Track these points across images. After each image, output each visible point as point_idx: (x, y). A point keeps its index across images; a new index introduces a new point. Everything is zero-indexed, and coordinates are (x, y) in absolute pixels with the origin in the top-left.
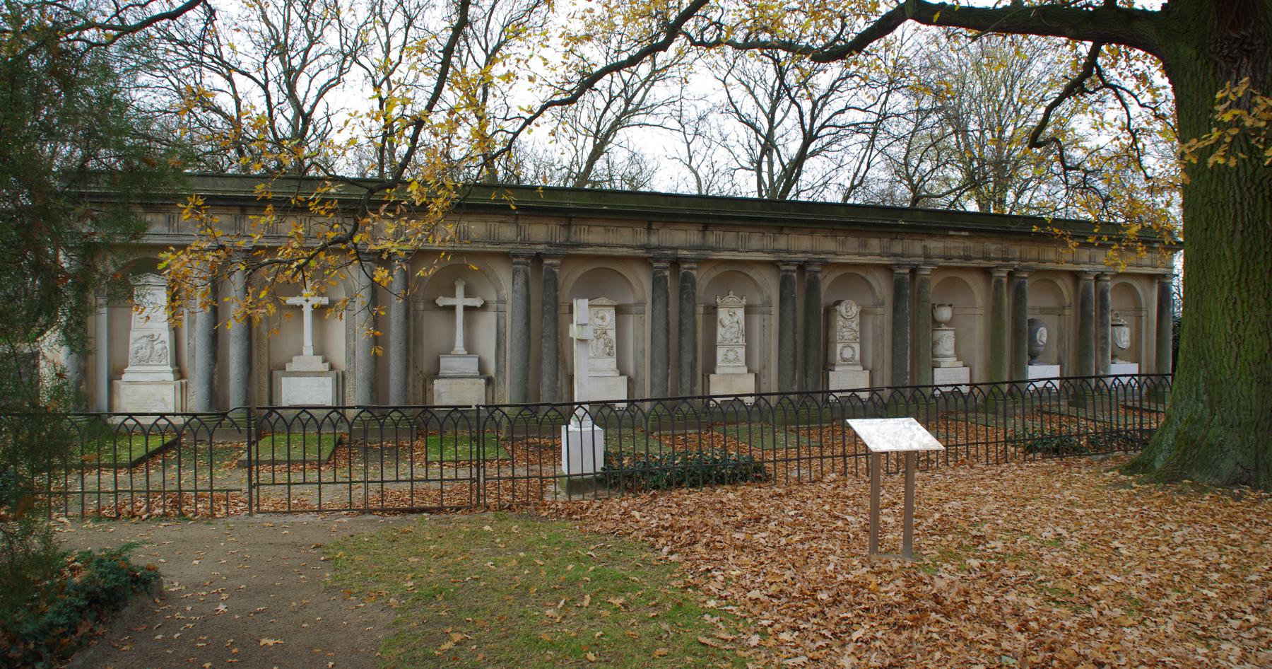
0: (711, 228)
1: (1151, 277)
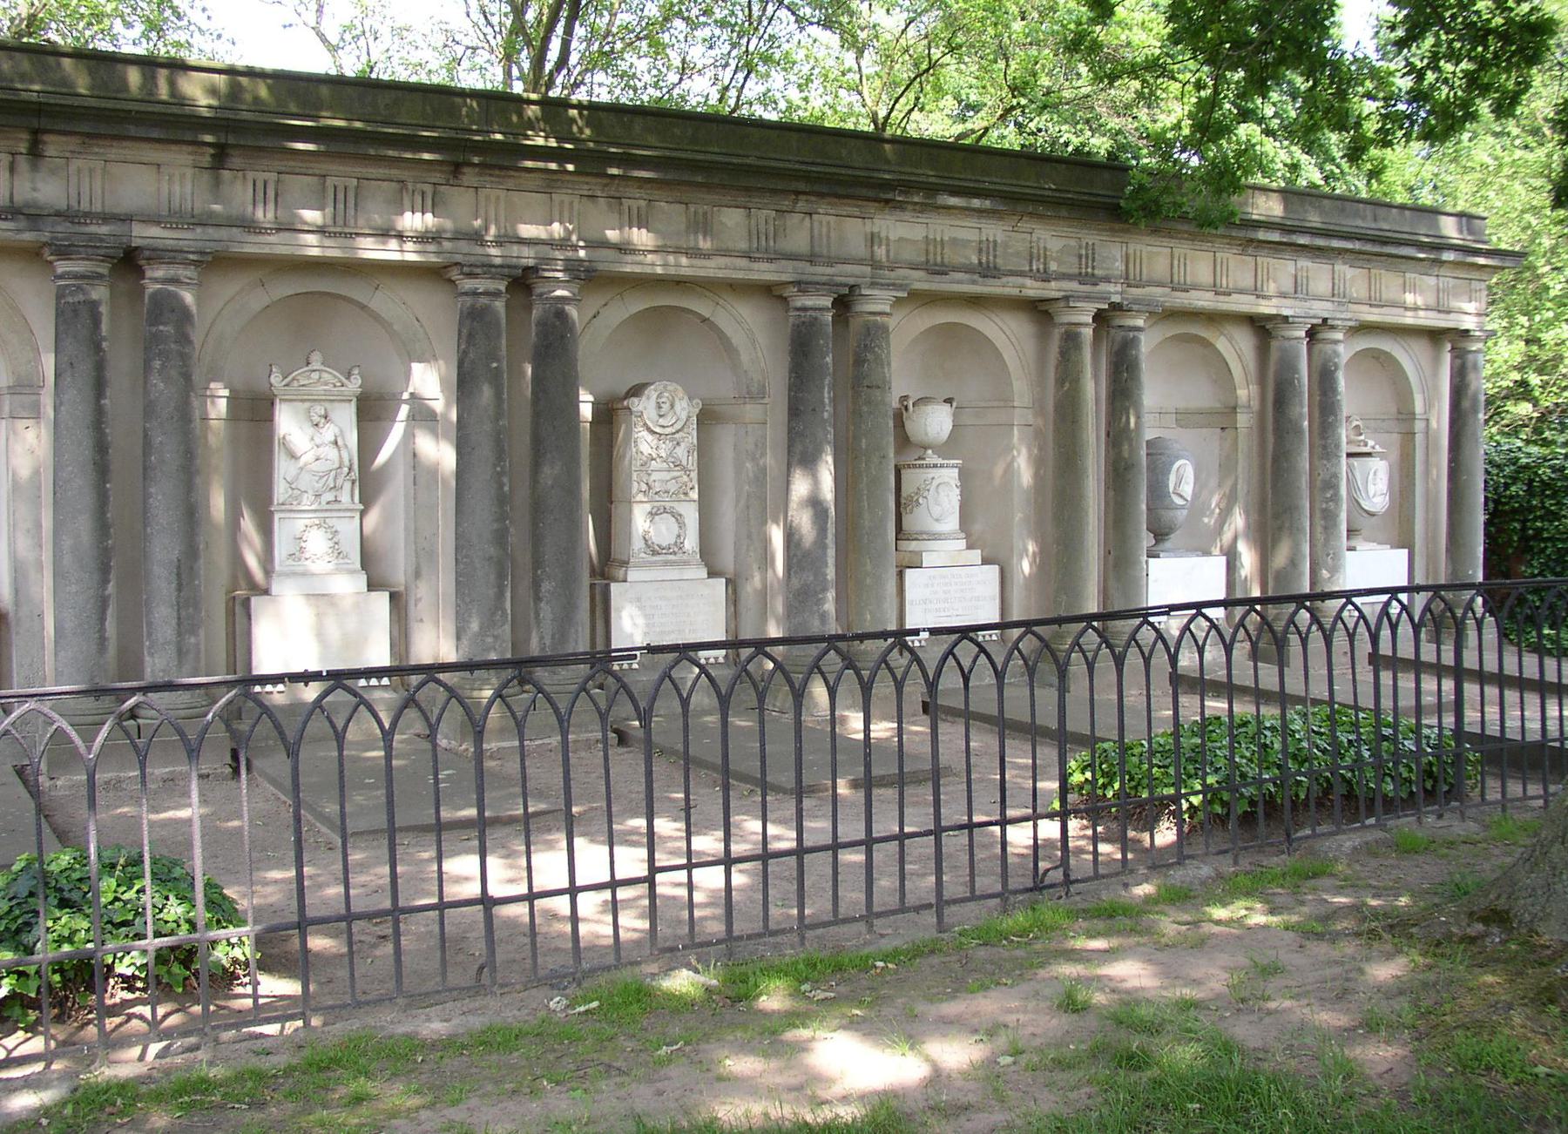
0: (236, 161)
1: (1435, 336)
